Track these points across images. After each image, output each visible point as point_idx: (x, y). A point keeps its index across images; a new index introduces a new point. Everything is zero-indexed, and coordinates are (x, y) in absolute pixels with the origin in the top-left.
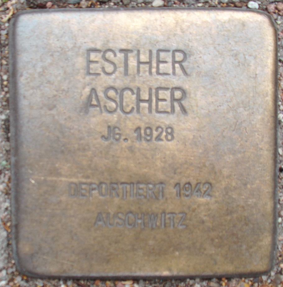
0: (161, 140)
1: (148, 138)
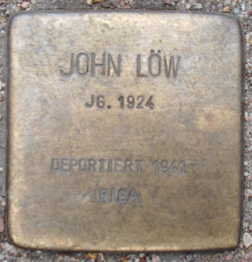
0: (142, 108)
1: (131, 105)
